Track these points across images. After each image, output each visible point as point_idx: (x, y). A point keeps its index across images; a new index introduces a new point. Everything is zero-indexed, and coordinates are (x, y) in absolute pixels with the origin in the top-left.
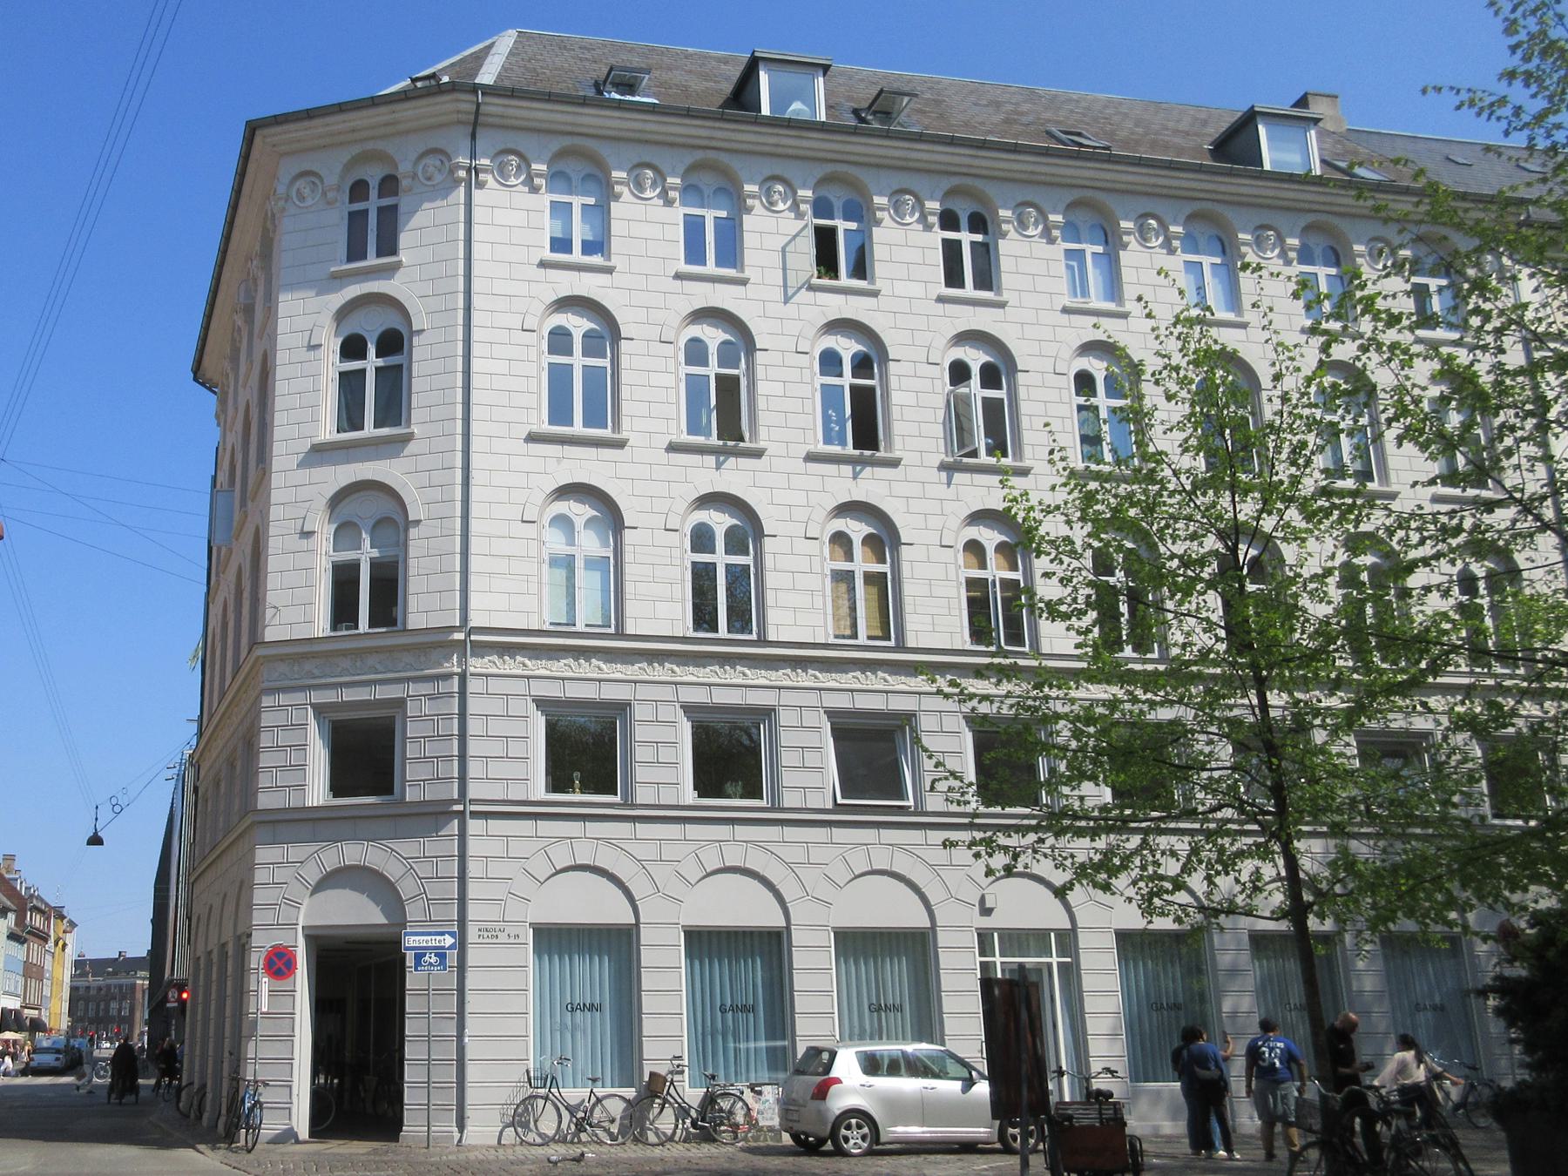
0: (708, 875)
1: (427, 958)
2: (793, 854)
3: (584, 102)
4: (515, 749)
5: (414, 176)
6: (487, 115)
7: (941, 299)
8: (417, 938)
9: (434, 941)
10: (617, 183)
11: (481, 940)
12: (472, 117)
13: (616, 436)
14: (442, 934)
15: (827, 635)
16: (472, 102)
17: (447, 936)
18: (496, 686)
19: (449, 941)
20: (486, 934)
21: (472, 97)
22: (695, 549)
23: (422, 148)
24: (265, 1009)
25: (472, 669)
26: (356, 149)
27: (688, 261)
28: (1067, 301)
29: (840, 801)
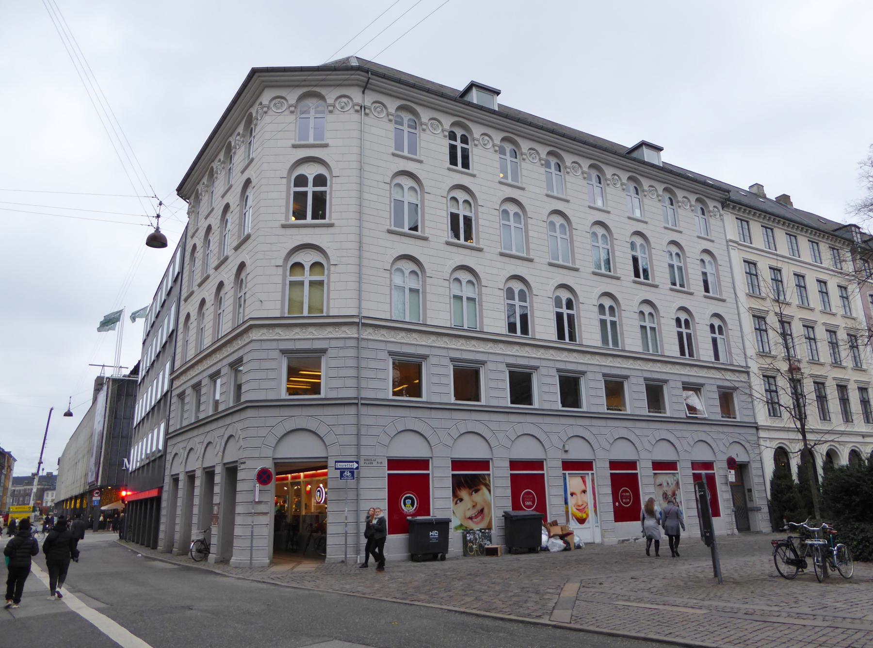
0: (518, 437)
1: (346, 473)
2: (547, 428)
3: (455, 100)
4: (381, 375)
5: (334, 106)
6: (371, 84)
8: (341, 464)
9: (349, 465)
10: (391, 115)
11: (365, 465)
12: (364, 84)
13: (423, 235)
14: (352, 462)
15: (451, 324)
16: (365, 77)
18: (371, 345)
19: (355, 465)
20: (367, 462)
21: (366, 74)
23: (339, 94)
24: (257, 500)
25: (362, 336)
26: (305, 90)
27: (451, 164)
29: (688, 415)
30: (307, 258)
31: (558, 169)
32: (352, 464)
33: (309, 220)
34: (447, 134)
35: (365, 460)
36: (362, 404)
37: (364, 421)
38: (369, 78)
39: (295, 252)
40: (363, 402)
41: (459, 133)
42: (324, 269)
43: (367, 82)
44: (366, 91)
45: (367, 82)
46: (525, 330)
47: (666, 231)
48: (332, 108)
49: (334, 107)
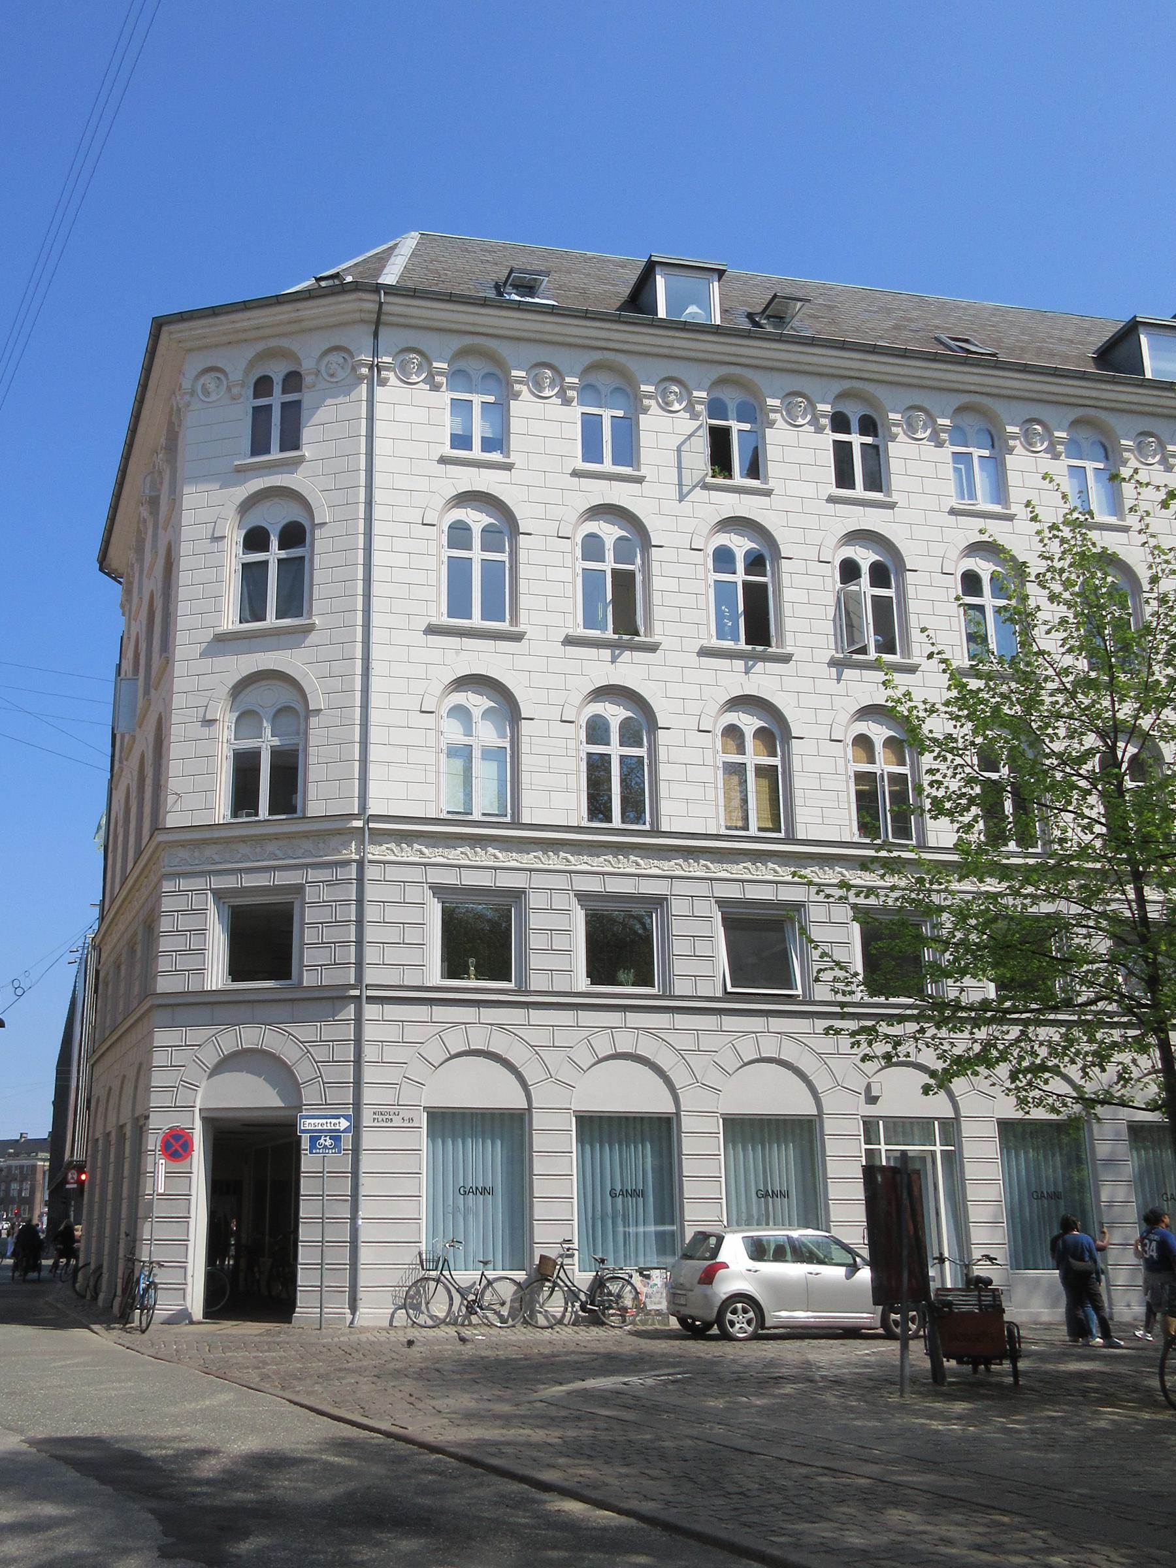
1: (322, 1141)
3: (484, 303)
4: (412, 936)
7: (832, 500)
14: (337, 1117)
17: (342, 1120)
18: (393, 873)
20: (380, 1118)
22: (591, 740)
24: (161, 1191)
25: (370, 857)
28: (954, 503)
30: (267, 697)
31: (1103, 455)
32: (337, 1121)
33: (271, 620)
34: (825, 421)
35: (375, 1113)
36: (368, 997)
37: (370, 1032)
38: (381, 304)
39: (249, 685)
40: (370, 993)
41: (854, 413)
42: (298, 717)
43: (380, 312)
44: (383, 332)
45: (380, 312)
46: (633, 806)
47: (452, 468)
48: (313, 377)
49: (317, 375)
